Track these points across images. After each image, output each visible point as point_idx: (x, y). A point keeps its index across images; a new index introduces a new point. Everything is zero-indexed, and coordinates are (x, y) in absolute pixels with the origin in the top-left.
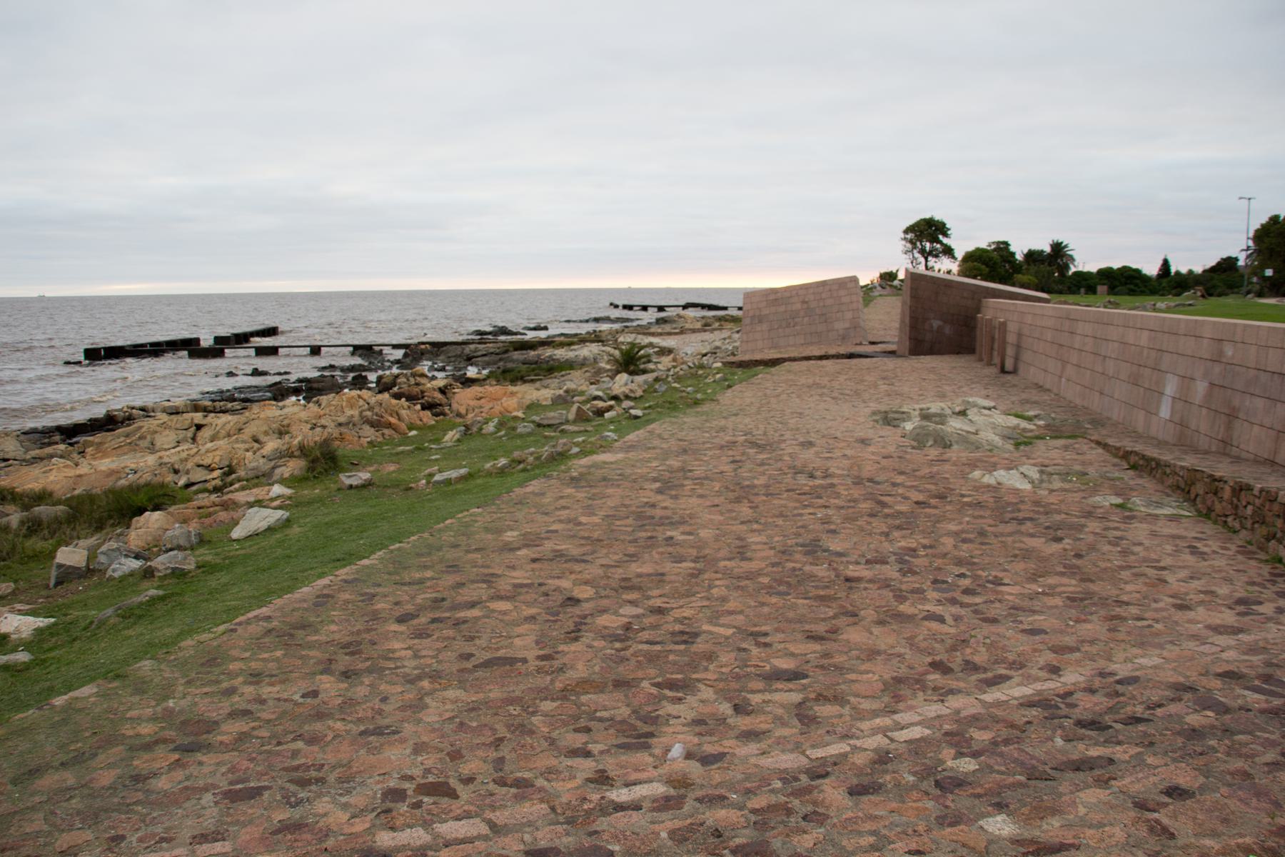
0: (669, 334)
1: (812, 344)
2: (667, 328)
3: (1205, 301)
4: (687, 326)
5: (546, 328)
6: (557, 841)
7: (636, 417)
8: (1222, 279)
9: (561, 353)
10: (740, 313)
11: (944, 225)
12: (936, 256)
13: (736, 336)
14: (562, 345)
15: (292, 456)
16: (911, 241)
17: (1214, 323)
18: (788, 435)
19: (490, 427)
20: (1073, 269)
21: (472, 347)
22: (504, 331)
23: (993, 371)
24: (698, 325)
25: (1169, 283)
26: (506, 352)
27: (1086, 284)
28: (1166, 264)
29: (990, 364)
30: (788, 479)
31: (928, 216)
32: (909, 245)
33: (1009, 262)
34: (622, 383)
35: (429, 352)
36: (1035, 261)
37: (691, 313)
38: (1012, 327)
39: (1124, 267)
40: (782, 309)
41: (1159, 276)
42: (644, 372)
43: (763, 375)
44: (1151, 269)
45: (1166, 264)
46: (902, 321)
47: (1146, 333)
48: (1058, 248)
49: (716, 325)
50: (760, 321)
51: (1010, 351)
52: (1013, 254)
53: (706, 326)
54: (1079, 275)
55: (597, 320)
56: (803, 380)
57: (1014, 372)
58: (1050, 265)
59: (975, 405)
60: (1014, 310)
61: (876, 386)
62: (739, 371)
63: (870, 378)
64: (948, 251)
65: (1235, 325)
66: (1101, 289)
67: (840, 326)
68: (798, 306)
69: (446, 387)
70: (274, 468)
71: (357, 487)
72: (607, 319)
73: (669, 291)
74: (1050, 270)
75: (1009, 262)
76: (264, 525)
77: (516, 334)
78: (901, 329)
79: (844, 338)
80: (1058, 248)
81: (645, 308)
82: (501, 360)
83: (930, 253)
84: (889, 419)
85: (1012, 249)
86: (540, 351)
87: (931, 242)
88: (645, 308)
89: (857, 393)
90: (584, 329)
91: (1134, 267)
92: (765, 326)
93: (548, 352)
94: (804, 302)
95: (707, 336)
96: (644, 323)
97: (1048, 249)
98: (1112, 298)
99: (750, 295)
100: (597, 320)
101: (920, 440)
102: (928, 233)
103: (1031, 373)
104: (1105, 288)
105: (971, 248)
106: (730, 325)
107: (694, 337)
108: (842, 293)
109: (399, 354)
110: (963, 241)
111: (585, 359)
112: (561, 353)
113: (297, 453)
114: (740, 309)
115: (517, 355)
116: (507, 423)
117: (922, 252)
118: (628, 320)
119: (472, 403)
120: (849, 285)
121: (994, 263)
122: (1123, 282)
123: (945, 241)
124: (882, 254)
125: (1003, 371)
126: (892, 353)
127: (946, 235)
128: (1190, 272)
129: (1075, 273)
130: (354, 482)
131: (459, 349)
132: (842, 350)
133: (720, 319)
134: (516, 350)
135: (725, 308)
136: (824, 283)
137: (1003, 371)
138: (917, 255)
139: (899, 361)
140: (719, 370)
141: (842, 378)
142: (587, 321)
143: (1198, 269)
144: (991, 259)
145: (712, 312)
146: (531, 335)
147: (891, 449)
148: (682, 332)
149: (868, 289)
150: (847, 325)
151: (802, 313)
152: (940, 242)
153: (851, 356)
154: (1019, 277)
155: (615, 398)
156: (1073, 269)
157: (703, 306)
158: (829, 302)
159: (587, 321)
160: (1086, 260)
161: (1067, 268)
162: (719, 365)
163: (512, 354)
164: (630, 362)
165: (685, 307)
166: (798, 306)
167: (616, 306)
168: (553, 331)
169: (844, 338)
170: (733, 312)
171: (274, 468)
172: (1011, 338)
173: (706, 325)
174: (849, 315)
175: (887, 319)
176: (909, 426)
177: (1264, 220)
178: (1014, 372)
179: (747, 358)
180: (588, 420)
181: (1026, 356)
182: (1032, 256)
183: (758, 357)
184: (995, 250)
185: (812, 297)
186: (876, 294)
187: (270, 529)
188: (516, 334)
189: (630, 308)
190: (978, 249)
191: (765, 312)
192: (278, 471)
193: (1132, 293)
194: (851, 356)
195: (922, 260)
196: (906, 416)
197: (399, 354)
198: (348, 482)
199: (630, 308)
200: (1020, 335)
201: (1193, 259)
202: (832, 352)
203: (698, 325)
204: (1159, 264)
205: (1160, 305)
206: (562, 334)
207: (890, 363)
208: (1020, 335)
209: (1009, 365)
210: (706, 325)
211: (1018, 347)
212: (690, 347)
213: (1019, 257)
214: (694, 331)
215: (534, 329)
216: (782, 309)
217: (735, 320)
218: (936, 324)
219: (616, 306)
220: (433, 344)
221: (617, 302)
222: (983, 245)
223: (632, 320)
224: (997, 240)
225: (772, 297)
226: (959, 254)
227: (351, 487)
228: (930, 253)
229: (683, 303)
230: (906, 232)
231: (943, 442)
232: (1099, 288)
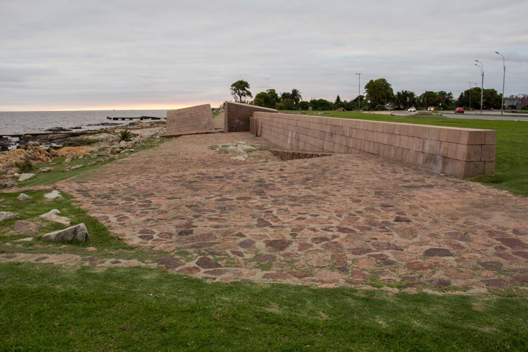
0: (137, 129)
1: (193, 130)
2: (135, 126)
3: (344, 112)
4: (144, 125)
5: (80, 128)
6: (143, 179)
7: (132, 151)
8: (356, 105)
9: (91, 137)
10: (166, 120)
11: (247, 83)
12: (244, 96)
13: (165, 129)
14: (91, 134)
15: (13, 166)
16: (234, 90)
17: (448, 130)
18: (181, 153)
19: (81, 157)
20: (301, 101)
21: (51, 135)
22: (61, 129)
23: (254, 135)
24: (149, 125)
25: (340, 106)
26: (67, 137)
27: (304, 106)
28: (338, 98)
29: (254, 134)
30: (181, 161)
31: (241, 80)
32: (234, 91)
33: (275, 98)
34: (123, 143)
35: (31, 138)
36: (286, 97)
37: (144, 121)
38: (260, 121)
39: (321, 100)
40: (182, 117)
41: (336, 103)
42: (130, 140)
43: (174, 139)
44: (332, 100)
45: (338, 98)
46: (225, 120)
47: (286, 120)
48: (295, 92)
49: (156, 125)
50: (174, 122)
51: (259, 129)
52: (276, 95)
53: (152, 125)
54: (303, 102)
55: (103, 124)
56: (188, 140)
57: (261, 136)
58: (291, 99)
59: (240, 143)
60: (263, 116)
61: (212, 141)
62: (166, 139)
63: (211, 139)
64: (249, 94)
65: (408, 127)
66: (310, 108)
67: (204, 123)
68: (188, 115)
69: (49, 149)
70: (7, 171)
71: (46, 172)
72: (108, 124)
73: (132, 111)
74: (291, 102)
75: (275, 98)
76: (28, 177)
77: (68, 130)
78: (225, 124)
79: (205, 127)
80: (295, 92)
81: (123, 119)
82: (66, 140)
83: (242, 94)
84: (212, 148)
85: (276, 92)
86: (81, 137)
87: (242, 90)
88: (123, 119)
89: (206, 143)
90: (98, 128)
91: (324, 99)
92: (175, 124)
93: (86, 137)
94: (190, 114)
95: (152, 129)
96: (124, 125)
97: (291, 93)
98: (303, 111)
99: (169, 112)
100: (103, 124)
101: (220, 152)
102: (241, 86)
103: (264, 136)
104: (312, 108)
105: (259, 92)
106: (162, 125)
107: (147, 130)
108: (204, 110)
109: (17, 139)
110: (256, 89)
111: (102, 139)
112: (91, 137)
113: (15, 166)
114: (166, 119)
115: (72, 138)
116: (75, 159)
117: (239, 94)
118: (116, 124)
119: (67, 153)
120: (207, 107)
121: (268, 100)
122: (320, 105)
123: (248, 89)
124: (220, 96)
125: (257, 136)
126: (222, 132)
127: (248, 87)
128: (345, 101)
129: (302, 102)
130: (45, 170)
131: (45, 137)
132: (204, 132)
133: (157, 123)
134: (71, 136)
135: (159, 119)
136: (197, 107)
137: (257, 136)
138: (237, 95)
139: (223, 134)
140: (159, 139)
141: (201, 139)
142: (98, 125)
143: (348, 101)
144: (267, 97)
145: (154, 120)
146: (74, 131)
147: (211, 154)
148: (142, 128)
149: (219, 109)
150: (206, 122)
151: (189, 118)
152: (246, 90)
153: (207, 133)
154: (277, 104)
155: (122, 148)
156: (301, 101)
157: (153, 118)
158: (199, 114)
159: (98, 125)
160: (306, 97)
161: (299, 100)
162: (159, 137)
163: (72, 138)
164: (125, 137)
165: (142, 119)
166: (188, 115)
167: (110, 119)
168: (85, 129)
169: (205, 127)
170: (163, 120)
171: (7, 171)
172: (260, 125)
173: (152, 125)
174: (207, 119)
175: (221, 121)
176: (218, 149)
177: (368, 82)
178: (261, 136)
179: (169, 135)
180: (115, 154)
181: (263, 130)
182: (285, 95)
183: (173, 134)
184: (269, 93)
185: (193, 112)
186: (221, 111)
187: (30, 179)
188: (68, 130)
189: (115, 119)
190: (262, 93)
191: (176, 118)
192: (8, 172)
193: (323, 109)
194: (207, 133)
195: (239, 97)
196: (217, 146)
197: (17, 139)
198: (43, 170)
199: (115, 119)
200: (262, 123)
201: (348, 98)
202: (201, 132)
203: (149, 125)
204: (335, 99)
205: (319, 113)
206: (89, 130)
207: (220, 135)
208: (262, 123)
209: (259, 134)
210: (152, 125)
211: (262, 127)
212: (147, 133)
213: (279, 96)
214: (147, 127)
215: (75, 128)
216: (182, 117)
217: (163, 123)
218: (237, 121)
219: (110, 119)
220: (32, 135)
221: (110, 117)
222: (265, 91)
223: (119, 124)
224: (270, 89)
225: (178, 112)
226: (254, 95)
227: (44, 172)
228: (242, 94)
229: (141, 117)
230: (232, 86)
231: (226, 152)
232: (309, 108)
